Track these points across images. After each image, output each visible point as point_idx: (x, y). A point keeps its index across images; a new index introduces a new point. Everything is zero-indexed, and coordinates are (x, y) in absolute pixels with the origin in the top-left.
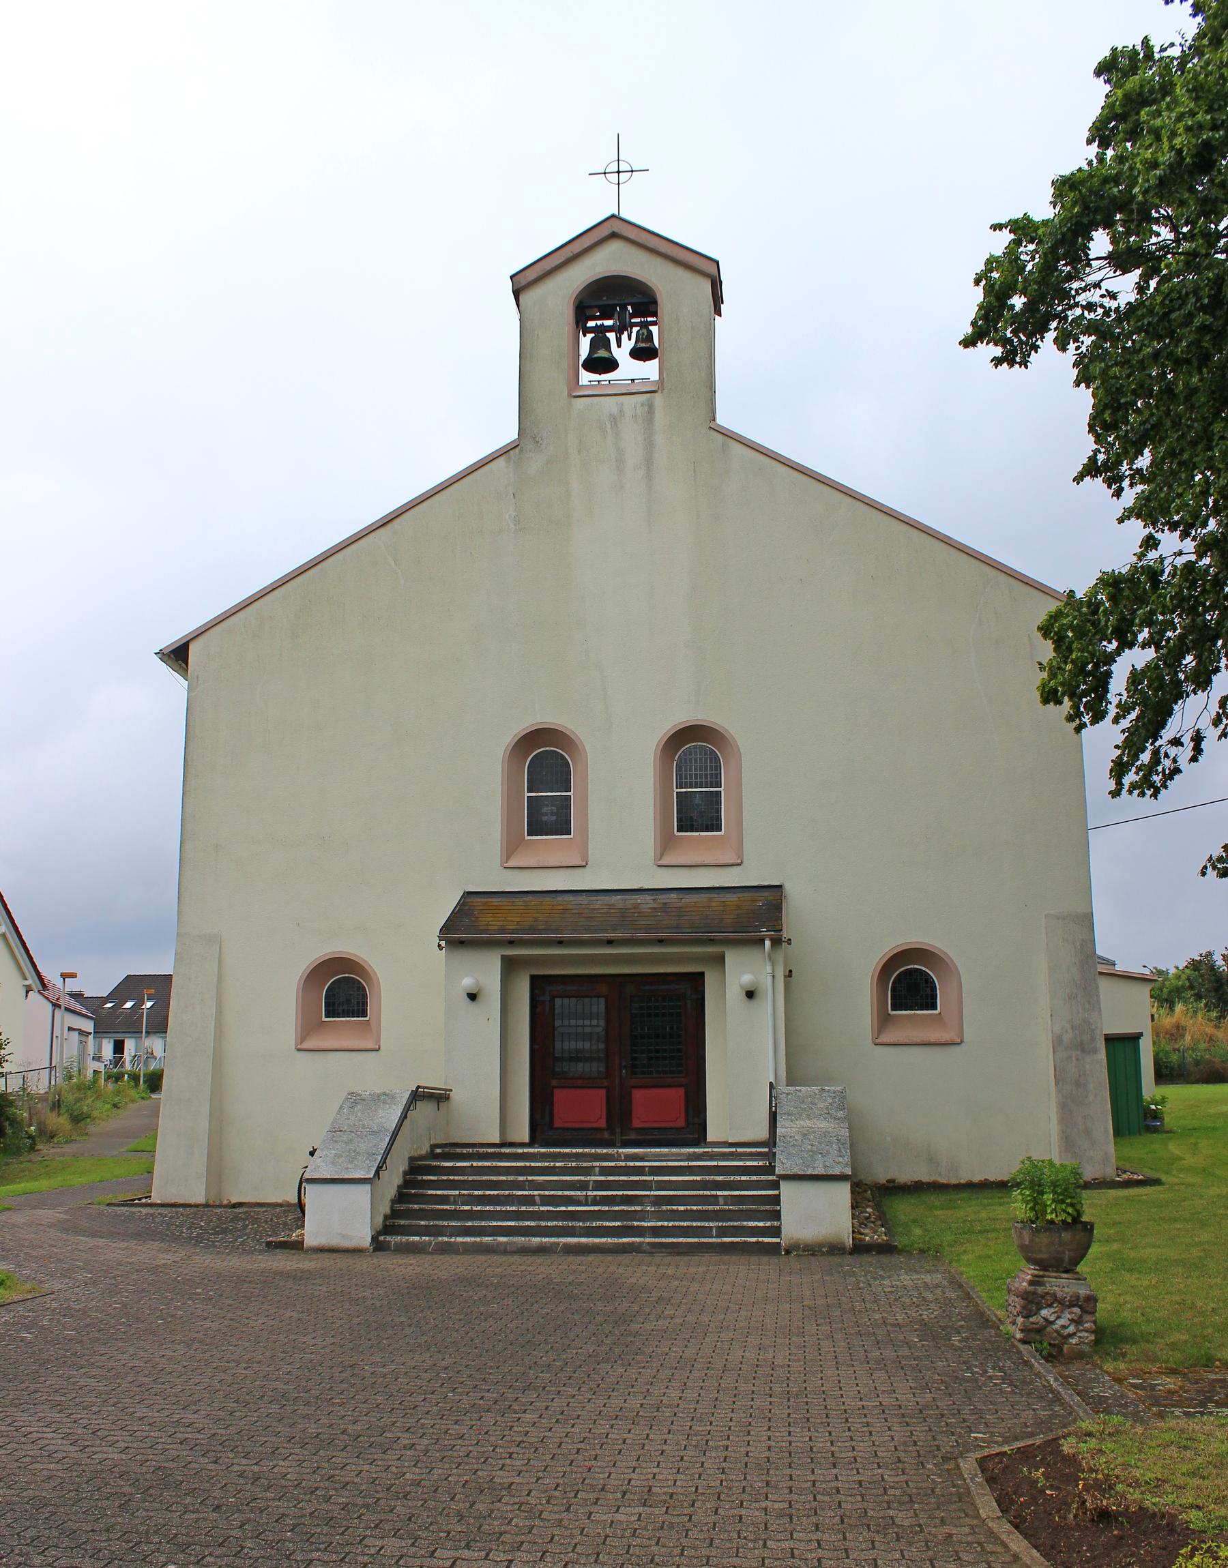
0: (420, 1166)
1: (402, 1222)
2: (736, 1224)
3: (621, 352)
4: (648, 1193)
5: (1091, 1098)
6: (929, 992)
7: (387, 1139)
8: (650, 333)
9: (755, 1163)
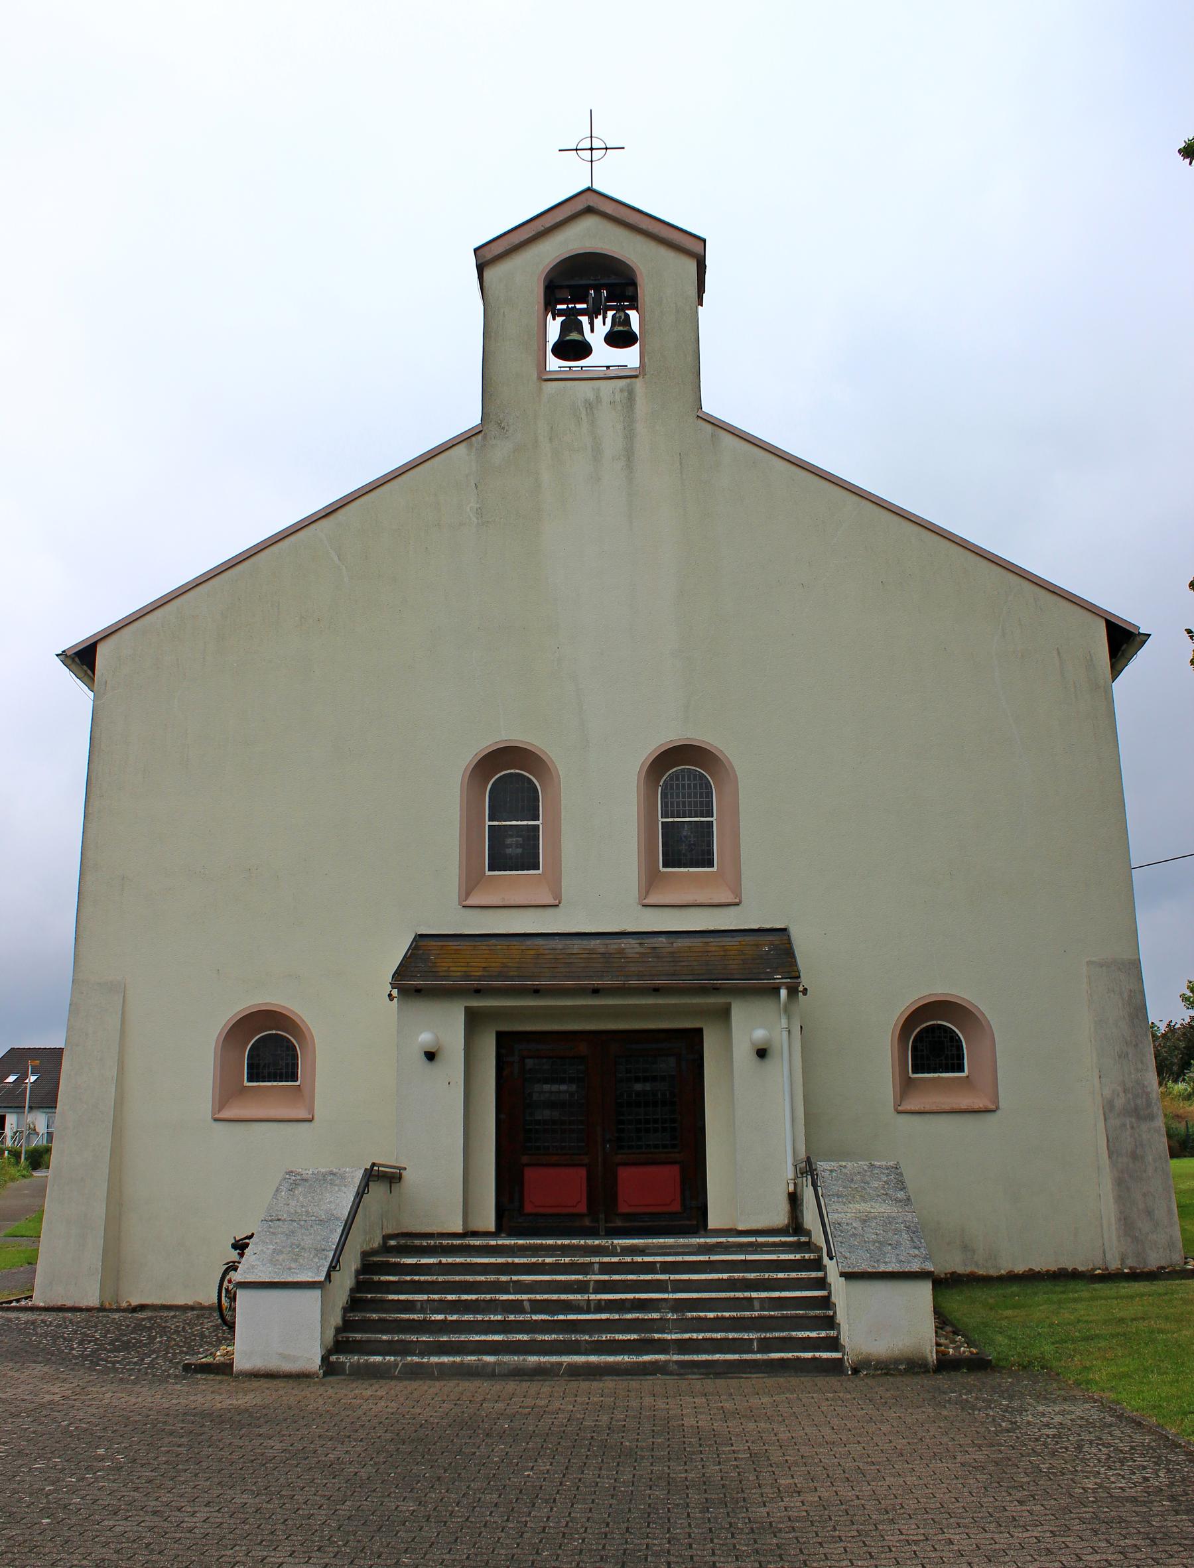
0: (375, 1264)
1: (358, 1336)
2: (782, 1334)
3: (596, 332)
4: (665, 1296)
6: (955, 1052)
7: (339, 1230)
8: (628, 317)
9: (791, 1257)
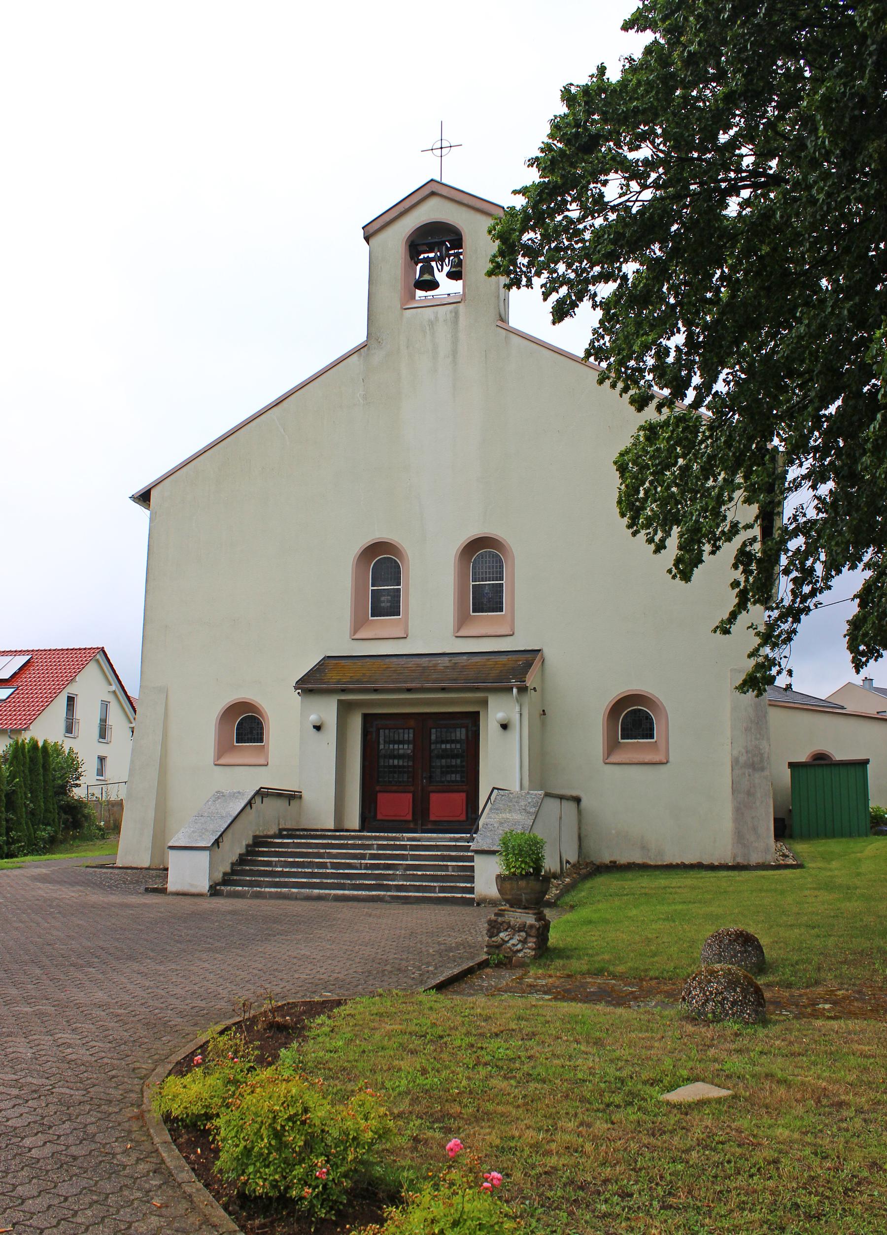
1: (235, 878)
3: (440, 276)
5: (758, 804)
6: (648, 726)
